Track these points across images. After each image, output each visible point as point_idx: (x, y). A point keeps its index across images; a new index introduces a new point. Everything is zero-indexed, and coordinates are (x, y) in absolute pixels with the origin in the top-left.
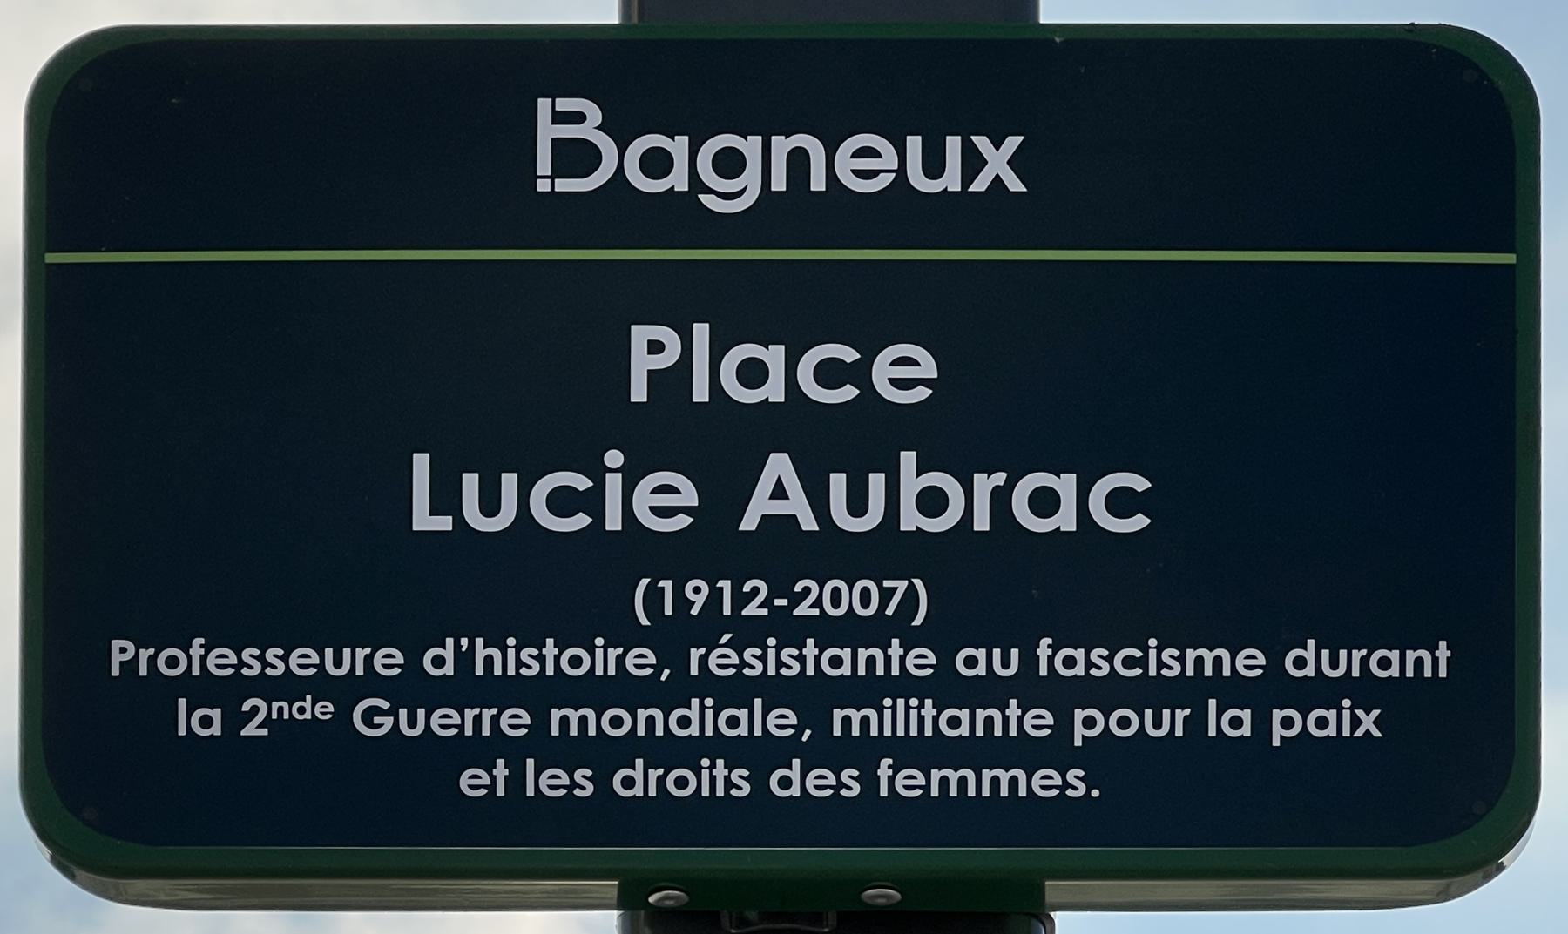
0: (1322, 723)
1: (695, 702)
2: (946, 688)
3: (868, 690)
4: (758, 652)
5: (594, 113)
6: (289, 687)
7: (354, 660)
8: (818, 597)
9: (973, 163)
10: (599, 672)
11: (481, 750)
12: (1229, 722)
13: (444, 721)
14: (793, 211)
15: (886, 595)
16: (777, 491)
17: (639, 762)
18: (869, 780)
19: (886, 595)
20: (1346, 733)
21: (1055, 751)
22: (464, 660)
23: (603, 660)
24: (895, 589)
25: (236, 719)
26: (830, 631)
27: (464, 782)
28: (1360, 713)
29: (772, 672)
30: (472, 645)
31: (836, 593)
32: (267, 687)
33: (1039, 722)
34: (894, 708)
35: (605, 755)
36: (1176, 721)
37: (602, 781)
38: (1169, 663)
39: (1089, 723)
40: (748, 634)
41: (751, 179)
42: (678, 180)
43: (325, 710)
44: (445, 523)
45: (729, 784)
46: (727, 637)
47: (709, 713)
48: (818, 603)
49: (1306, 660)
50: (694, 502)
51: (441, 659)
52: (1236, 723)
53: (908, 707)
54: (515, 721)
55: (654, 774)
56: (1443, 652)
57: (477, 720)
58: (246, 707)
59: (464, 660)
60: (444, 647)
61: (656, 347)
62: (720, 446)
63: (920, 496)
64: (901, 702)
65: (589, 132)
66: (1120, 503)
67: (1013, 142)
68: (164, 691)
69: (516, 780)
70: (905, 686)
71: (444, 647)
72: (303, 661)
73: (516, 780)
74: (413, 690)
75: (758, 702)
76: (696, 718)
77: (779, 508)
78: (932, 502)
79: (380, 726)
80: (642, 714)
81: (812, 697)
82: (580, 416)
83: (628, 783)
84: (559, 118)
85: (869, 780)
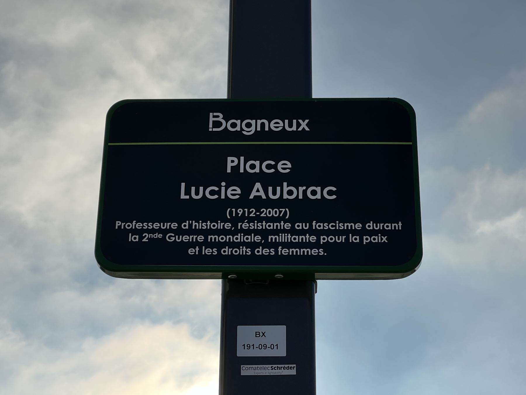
0: (374, 239)
2: (293, 232)
3: (276, 232)
6: (153, 231)
7: (167, 225)
8: (265, 212)
9: (299, 125)
10: (219, 228)
11: (193, 244)
12: (354, 239)
13: (185, 238)
14: (261, 135)
15: (280, 212)
16: (257, 190)
18: (276, 251)
19: (280, 212)
20: (380, 241)
21: (317, 245)
22: (190, 225)
23: (220, 225)
25: (141, 238)
26: (268, 220)
27: (189, 251)
29: (256, 228)
30: (192, 222)
31: (270, 212)
32: (148, 231)
34: (282, 236)
35: (220, 246)
38: (341, 226)
39: (324, 239)
40: (251, 220)
41: (253, 128)
42: (238, 128)
43: (160, 236)
45: (246, 252)
46: (246, 221)
47: (242, 237)
48: (266, 214)
49: (370, 226)
51: (185, 225)
52: (135, 238)
53: (285, 236)
55: (230, 250)
56: (400, 224)
57: (193, 238)
59: (190, 225)
62: (245, 181)
63: (287, 191)
64: (283, 235)
65: (220, 119)
66: (330, 193)
67: (307, 121)
68: (126, 232)
69: (200, 251)
70: (284, 231)
72: (156, 226)
73: (200, 251)
74: (179, 232)
75: (253, 234)
76: (239, 238)
77: (258, 194)
78: (290, 193)
81: (264, 233)
82: (217, 175)
84: (214, 117)
85: (276, 251)
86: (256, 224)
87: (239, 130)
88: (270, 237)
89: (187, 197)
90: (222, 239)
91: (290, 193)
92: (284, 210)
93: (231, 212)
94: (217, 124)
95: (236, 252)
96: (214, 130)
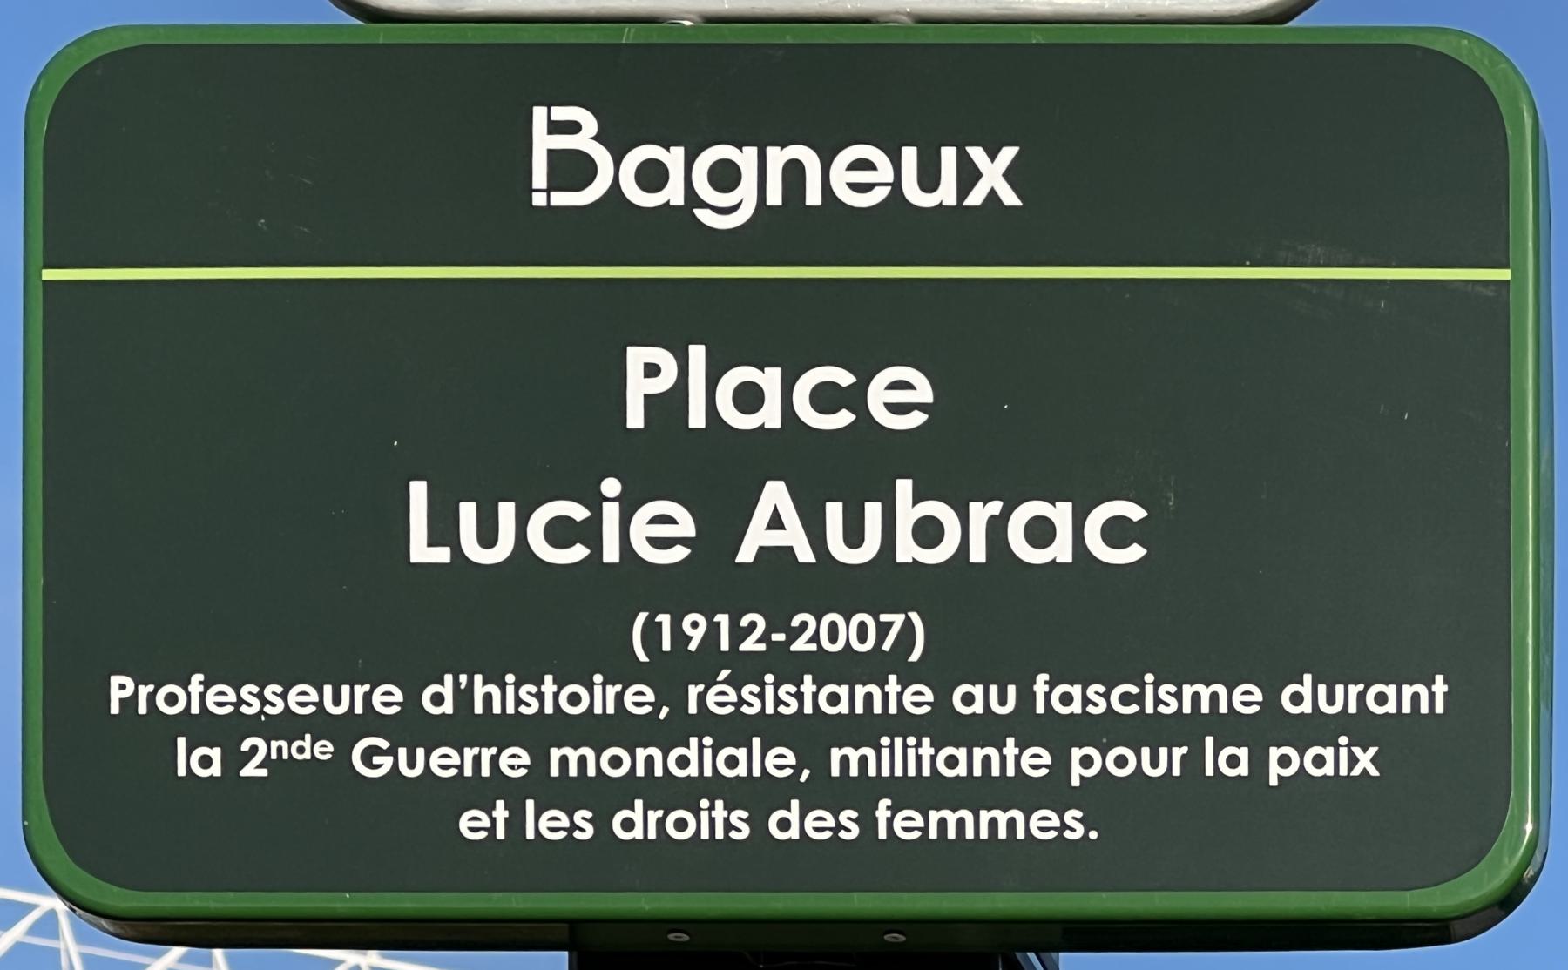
2: (944, 726)
4: (756, 689)
6: (288, 726)
7: (353, 698)
8: (819, 631)
9: (968, 175)
11: (481, 791)
12: (1226, 761)
13: (443, 761)
14: (788, 227)
15: (883, 629)
16: (773, 522)
17: (639, 804)
18: (867, 822)
19: (883, 629)
20: (1343, 772)
22: (464, 697)
23: (602, 698)
24: (890, 624)
25: (235, 759)
26: (832, 667)
27: (464, 824)
29: (770, 710)
30: (471, 682)
33: (1036, 761)
34: (891, 747)
35: (604, 796)
37: (602, 823)
38: (1166, 699)
40: (746, 670)
41: (746, 192)
42: (673, 194)
43: (324, 750)
44: (442, 555)
45: (728, 826)
46: (724, 674)
47: (708, 753)
48: (815, 638)
49: (1304, 696)
51: (439, 699)
52: (1233, 761)
53: (905, 747)
54: (514, 762)
55: (654, 816)
56: (1440, 687)
57: (477, 760)
58: (245, 746)
59: (464, 697)
61: (652, 370)
62: (715, 473)
65: (584, 142)
66: (1116, 532)
67: (1008, 154)
69: (516, 822)
70: (903, 724)
72: (302, 699)
73: (516, 822)
74: (413, 729)
75: (756, 742)
76: (695, 758)
77: (776, 539)
78: (928, 532)
80: (641, 753)
81: (812, 736)
82: (573, 442)
84: (555, 128)
85: (867, 822)
88: (836, 754)
89: (884, 618)
91: (928, 532)
92: (898, 619)
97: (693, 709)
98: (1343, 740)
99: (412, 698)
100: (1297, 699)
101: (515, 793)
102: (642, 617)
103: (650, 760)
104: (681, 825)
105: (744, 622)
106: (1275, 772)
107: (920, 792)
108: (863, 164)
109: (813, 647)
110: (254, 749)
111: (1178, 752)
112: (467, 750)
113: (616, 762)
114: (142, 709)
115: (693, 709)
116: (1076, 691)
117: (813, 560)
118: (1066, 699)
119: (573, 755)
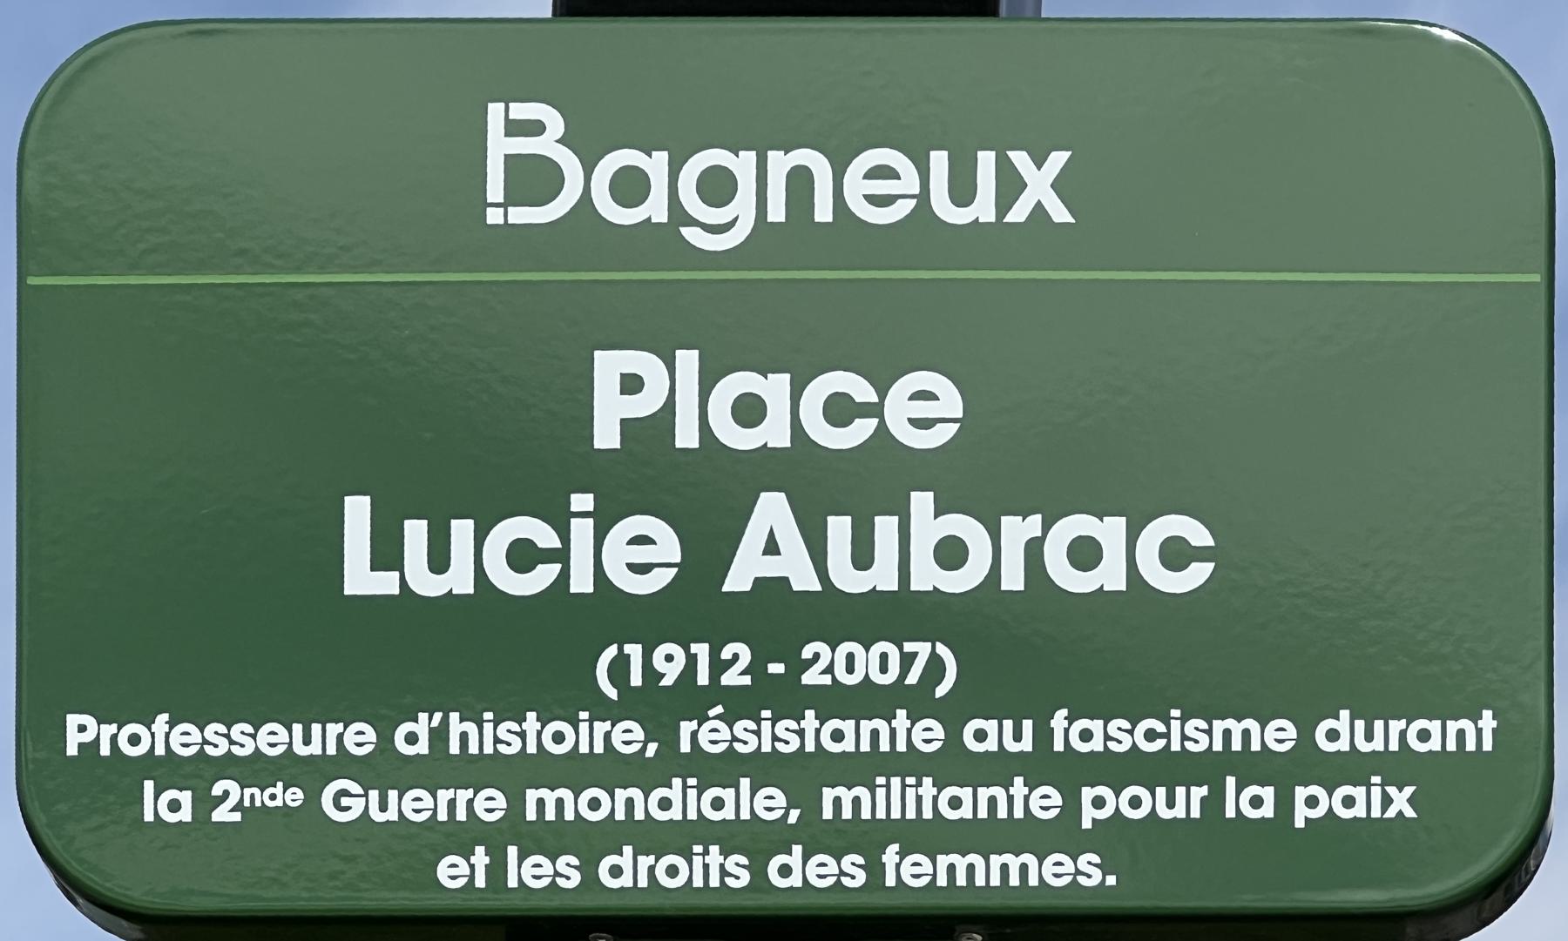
0: (1349, 802)
1: (677, 782)
2: (952, 765)
3: (863, 768)
4: (752, 726)
5: (555, 123)
6: (255, 770)
7: (323, 739)
8: (828, 662)
9: (1010, 186)
11: (460, 836)
12: (1251, 802)
13: (415, 805)
14: (790, 237)
15: (907, 660)
18: (874, 869)
19: (907, 660)
22: (439, 736)
23: (587, 736)
24: (915, 655)
25: (204, 804)
28: (1392, 790)
29: (766, 748)
30: (445, 721)
33: (1046, 802)
34: (888, 786)
35: (591, 842)
36: (1189, 802)
37: (588, 870)
39: (1099, 803)
40: (739, 705)
41: (743, 207)
42: (655, 209)
43: (295, 797)
45: (724, 872)
46: (719, 709)
48: (829, 670)
49: (1341, 732)
50: (677, 557)
51: (414, 736)
52: (1256, 802)
53: (904, 786)
55: (645, 861)
56: (1488, 721)
57: (452, 804)
59: (439, 736)
60: (1338, 718)
61: (631, 384)
62: (701, 492)
63: (922, 549)
65: (547, 145)
66: (1176, 554)
67: (1058, 159)
69: (497, 870)
70: (910, 764)
71: (1338, 718)
73: (497, 870)
74: (383, 770)
75: (745, 783)
76: (679, 800)
77: (771, 568)
78: (951, 553)
79: (348, 808)
81: (802, 774)
82: (536, 460)
83: (616, 871)
84: (514, 128)
85: (874, 869)
86: (766, 725)
87: (661, 216)
88: (828, 794)
89: (909, 647)
90: (614, 804)
91: (951, 553)
92: (923, 649)
93: (620, 668)
94: (531, 179)
95: (672, 871)
96: (521, 215)
97: (685, 747)
98: (1376, 779)
99: (385, 739)
100: (1333, 735)
101: (495, 838)
102: (612, 651)
103: (630, 803)
104: (672, 871)
105: (726, 654)
106: (1301, 815)
107: (927, 836)
108: (882, 172)
109: (826, 680)
110: (226, 794)
111: (1199, 792)
112: (441, 793)
113: (594, 804)
114: (105, 750)
115: (685, 747)
116: (1096, 726)
117: (725, 589)
118: (1086, 736)
119: (550, 797)
